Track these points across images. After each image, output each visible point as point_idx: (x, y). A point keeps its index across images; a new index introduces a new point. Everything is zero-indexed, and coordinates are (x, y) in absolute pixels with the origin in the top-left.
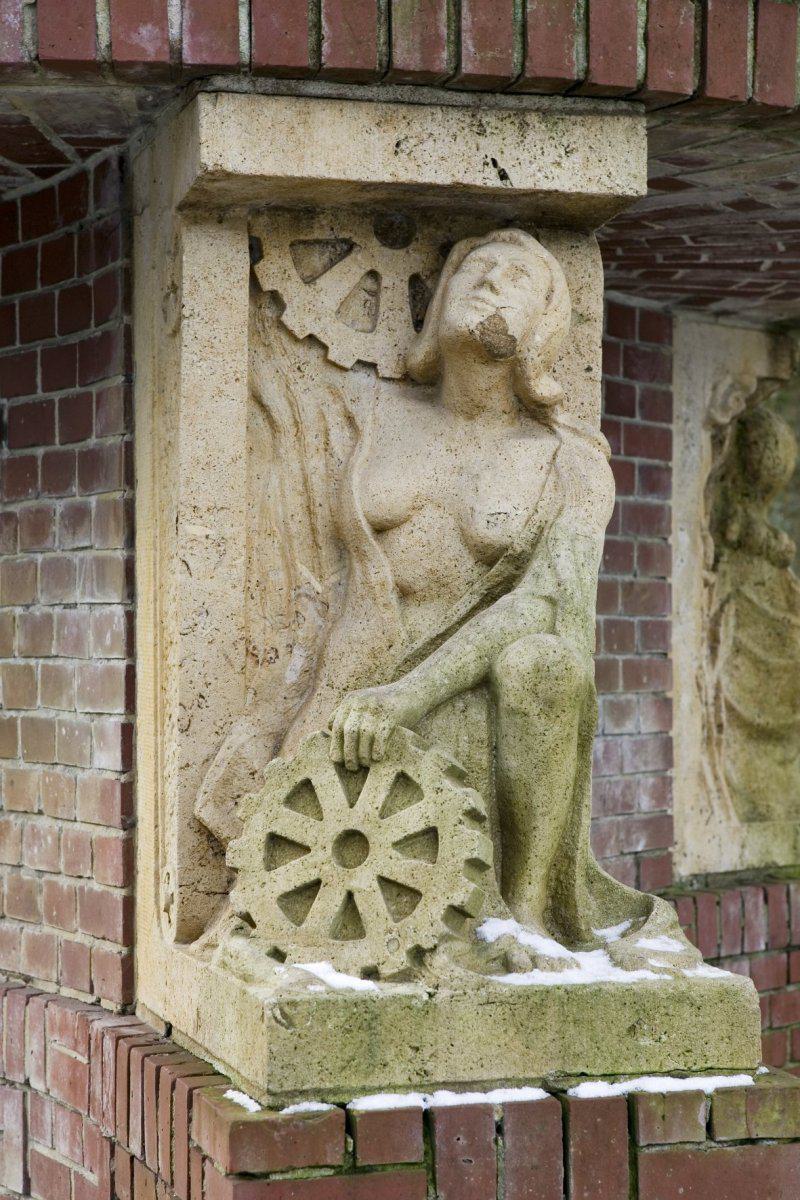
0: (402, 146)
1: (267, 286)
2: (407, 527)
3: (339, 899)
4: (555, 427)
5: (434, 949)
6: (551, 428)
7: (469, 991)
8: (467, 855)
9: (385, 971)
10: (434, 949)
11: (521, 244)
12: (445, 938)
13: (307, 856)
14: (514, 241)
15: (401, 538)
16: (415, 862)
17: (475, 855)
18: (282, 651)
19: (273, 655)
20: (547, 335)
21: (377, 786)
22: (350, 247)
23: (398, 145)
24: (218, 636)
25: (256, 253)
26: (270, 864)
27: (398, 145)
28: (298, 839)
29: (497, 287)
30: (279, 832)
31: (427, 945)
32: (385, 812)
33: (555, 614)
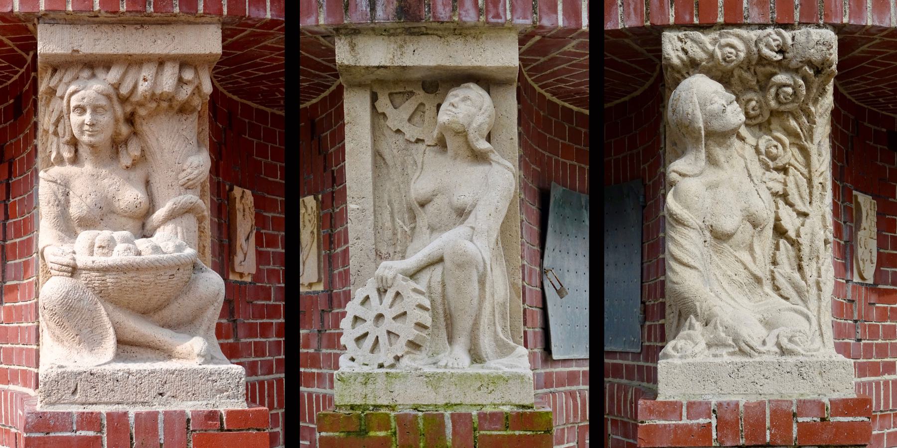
0: (416, 51)
1: (380, 111)
2: (431, 204)
3: (374, 339)
4: (492, 162)
5: (402, 356)
6: (104, 95)
7: (412, 371)
8: (415, 321)
9: (386, 365)
10: (402, 356)
11: (472, 89)
12: (407, 353)
13: (365, 324)
14: (469, 87)
15: (430, 208)
16: (694, 400)
17: (418, 321)
18: (392, 254)
19: (388, 255)
20: (478, 123)
21: (389, 296)
22: (411, 94)
23: (414, 51)
24: (364, 248)
25: (374, 98)
26: (353, 327)
27: (414, 51)
28: (363, 318)
29: (455, 105)
30: (358, 315)
31: (399, 355)
32: (391, 306)
33: (473, 232)
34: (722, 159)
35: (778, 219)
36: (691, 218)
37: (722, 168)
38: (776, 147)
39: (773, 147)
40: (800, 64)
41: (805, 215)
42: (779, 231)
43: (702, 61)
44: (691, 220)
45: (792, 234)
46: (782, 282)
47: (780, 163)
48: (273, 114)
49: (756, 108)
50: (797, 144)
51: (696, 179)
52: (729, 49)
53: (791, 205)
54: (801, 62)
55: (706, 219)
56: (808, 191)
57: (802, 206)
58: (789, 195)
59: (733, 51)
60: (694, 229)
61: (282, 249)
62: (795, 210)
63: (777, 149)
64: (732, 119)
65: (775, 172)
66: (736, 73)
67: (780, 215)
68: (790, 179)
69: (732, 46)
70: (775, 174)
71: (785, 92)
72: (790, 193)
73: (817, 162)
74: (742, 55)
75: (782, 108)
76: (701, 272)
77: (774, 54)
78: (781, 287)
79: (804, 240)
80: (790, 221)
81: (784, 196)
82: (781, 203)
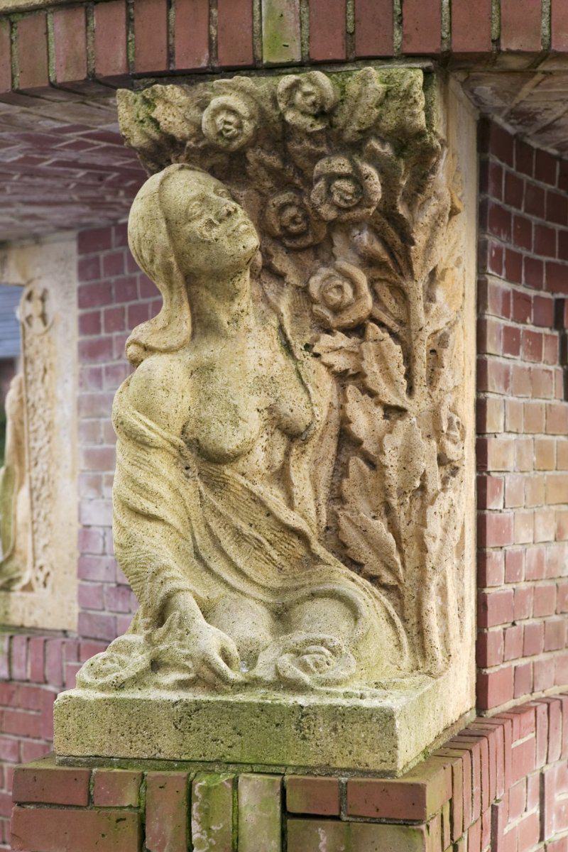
34: (224, 318)
35: (345, 421)
36: (150, 428)
37: (226, 336)
38: (340, 288)
39: (334, 290)
40: (360, 136)
41: (401, 411)
42: (346, 439)
43: (185, 140)
44: (148, 432)
45: (369, 446)
46: (351, 535)
47: (348, 318)
48: (529, 249)
49: (299, 220)
50: (386, 280)
51: (165, 358)
52: (223, 116)
53: (372, 394)
54: (360, 132)
55: (189, 427)
56: (403, 368)
57: (392, 396)
58: (365, 376)
59: (231, 118)
60: (157, 448)
61: (9, 790)
62: (379, 403)
63: (343, 292)
64: (227, 247)
65: (340, 335)
66: (251, 156)
67: (349, 413)
68: (369, 349)
69: (232, 111)
70: (341, 340)
71: (338, 189)
72: (368, 372)
73: (422, 314)
74: (248, 127)
75: (345, 216)
76: (170, 525)
77: (310, 120)
78: (349, 544)
79: (391, 459)
80: (364, 421)
81: (358, 376)
82: (351, 389)
